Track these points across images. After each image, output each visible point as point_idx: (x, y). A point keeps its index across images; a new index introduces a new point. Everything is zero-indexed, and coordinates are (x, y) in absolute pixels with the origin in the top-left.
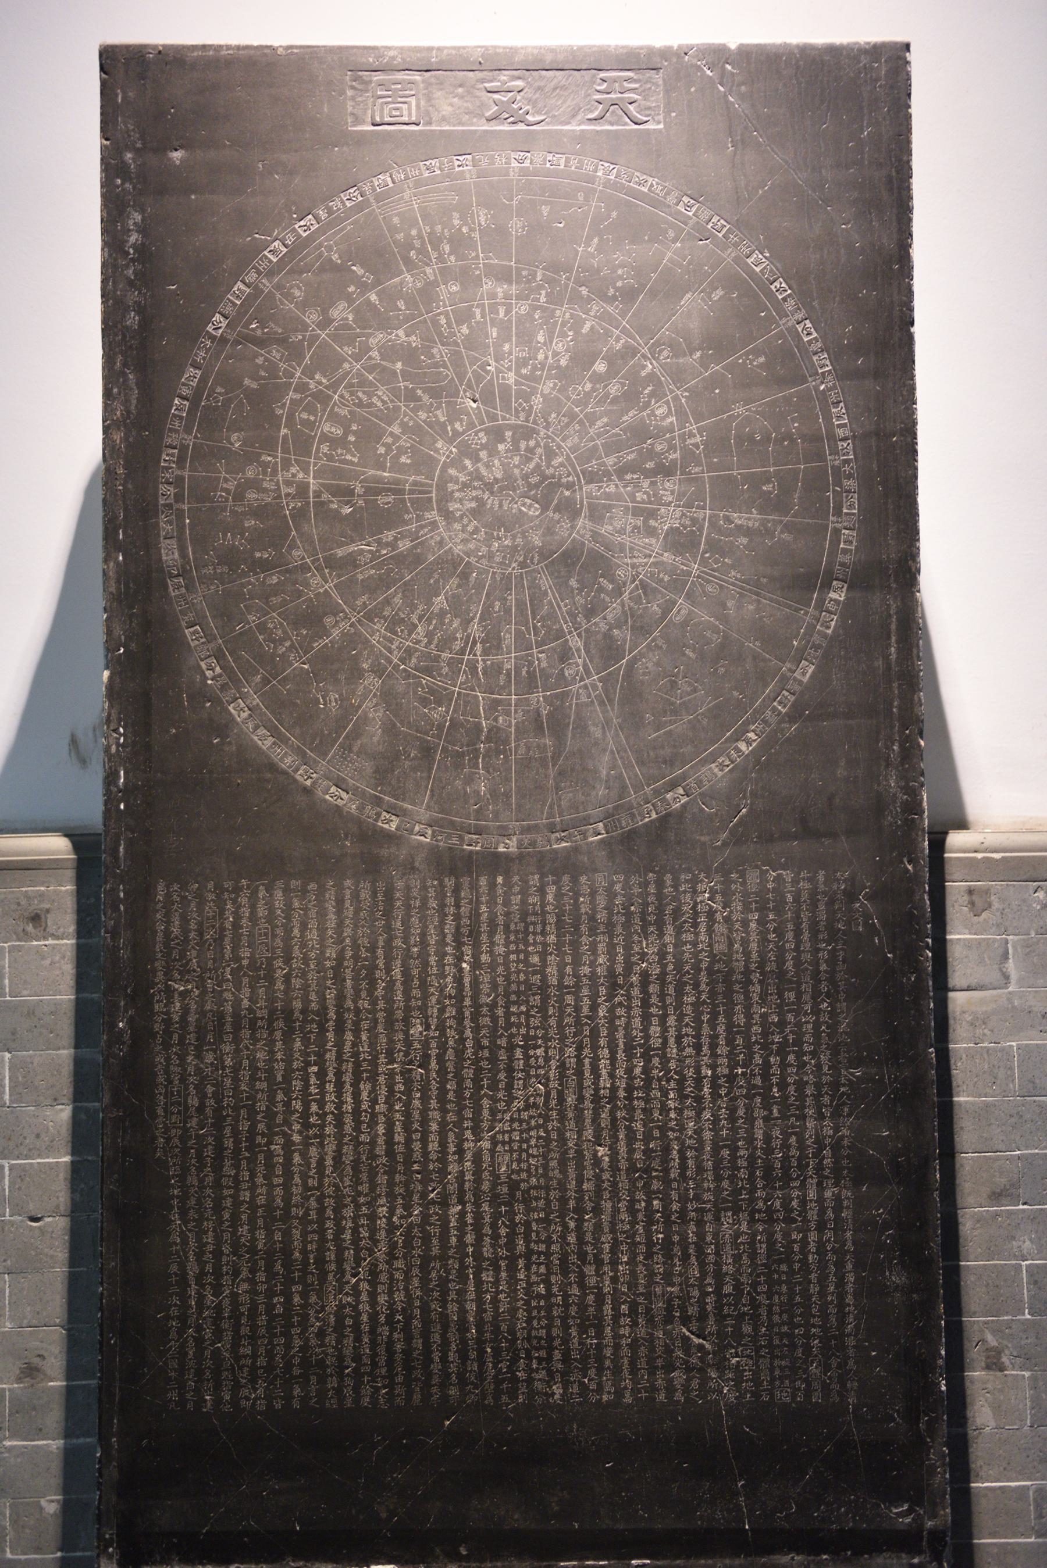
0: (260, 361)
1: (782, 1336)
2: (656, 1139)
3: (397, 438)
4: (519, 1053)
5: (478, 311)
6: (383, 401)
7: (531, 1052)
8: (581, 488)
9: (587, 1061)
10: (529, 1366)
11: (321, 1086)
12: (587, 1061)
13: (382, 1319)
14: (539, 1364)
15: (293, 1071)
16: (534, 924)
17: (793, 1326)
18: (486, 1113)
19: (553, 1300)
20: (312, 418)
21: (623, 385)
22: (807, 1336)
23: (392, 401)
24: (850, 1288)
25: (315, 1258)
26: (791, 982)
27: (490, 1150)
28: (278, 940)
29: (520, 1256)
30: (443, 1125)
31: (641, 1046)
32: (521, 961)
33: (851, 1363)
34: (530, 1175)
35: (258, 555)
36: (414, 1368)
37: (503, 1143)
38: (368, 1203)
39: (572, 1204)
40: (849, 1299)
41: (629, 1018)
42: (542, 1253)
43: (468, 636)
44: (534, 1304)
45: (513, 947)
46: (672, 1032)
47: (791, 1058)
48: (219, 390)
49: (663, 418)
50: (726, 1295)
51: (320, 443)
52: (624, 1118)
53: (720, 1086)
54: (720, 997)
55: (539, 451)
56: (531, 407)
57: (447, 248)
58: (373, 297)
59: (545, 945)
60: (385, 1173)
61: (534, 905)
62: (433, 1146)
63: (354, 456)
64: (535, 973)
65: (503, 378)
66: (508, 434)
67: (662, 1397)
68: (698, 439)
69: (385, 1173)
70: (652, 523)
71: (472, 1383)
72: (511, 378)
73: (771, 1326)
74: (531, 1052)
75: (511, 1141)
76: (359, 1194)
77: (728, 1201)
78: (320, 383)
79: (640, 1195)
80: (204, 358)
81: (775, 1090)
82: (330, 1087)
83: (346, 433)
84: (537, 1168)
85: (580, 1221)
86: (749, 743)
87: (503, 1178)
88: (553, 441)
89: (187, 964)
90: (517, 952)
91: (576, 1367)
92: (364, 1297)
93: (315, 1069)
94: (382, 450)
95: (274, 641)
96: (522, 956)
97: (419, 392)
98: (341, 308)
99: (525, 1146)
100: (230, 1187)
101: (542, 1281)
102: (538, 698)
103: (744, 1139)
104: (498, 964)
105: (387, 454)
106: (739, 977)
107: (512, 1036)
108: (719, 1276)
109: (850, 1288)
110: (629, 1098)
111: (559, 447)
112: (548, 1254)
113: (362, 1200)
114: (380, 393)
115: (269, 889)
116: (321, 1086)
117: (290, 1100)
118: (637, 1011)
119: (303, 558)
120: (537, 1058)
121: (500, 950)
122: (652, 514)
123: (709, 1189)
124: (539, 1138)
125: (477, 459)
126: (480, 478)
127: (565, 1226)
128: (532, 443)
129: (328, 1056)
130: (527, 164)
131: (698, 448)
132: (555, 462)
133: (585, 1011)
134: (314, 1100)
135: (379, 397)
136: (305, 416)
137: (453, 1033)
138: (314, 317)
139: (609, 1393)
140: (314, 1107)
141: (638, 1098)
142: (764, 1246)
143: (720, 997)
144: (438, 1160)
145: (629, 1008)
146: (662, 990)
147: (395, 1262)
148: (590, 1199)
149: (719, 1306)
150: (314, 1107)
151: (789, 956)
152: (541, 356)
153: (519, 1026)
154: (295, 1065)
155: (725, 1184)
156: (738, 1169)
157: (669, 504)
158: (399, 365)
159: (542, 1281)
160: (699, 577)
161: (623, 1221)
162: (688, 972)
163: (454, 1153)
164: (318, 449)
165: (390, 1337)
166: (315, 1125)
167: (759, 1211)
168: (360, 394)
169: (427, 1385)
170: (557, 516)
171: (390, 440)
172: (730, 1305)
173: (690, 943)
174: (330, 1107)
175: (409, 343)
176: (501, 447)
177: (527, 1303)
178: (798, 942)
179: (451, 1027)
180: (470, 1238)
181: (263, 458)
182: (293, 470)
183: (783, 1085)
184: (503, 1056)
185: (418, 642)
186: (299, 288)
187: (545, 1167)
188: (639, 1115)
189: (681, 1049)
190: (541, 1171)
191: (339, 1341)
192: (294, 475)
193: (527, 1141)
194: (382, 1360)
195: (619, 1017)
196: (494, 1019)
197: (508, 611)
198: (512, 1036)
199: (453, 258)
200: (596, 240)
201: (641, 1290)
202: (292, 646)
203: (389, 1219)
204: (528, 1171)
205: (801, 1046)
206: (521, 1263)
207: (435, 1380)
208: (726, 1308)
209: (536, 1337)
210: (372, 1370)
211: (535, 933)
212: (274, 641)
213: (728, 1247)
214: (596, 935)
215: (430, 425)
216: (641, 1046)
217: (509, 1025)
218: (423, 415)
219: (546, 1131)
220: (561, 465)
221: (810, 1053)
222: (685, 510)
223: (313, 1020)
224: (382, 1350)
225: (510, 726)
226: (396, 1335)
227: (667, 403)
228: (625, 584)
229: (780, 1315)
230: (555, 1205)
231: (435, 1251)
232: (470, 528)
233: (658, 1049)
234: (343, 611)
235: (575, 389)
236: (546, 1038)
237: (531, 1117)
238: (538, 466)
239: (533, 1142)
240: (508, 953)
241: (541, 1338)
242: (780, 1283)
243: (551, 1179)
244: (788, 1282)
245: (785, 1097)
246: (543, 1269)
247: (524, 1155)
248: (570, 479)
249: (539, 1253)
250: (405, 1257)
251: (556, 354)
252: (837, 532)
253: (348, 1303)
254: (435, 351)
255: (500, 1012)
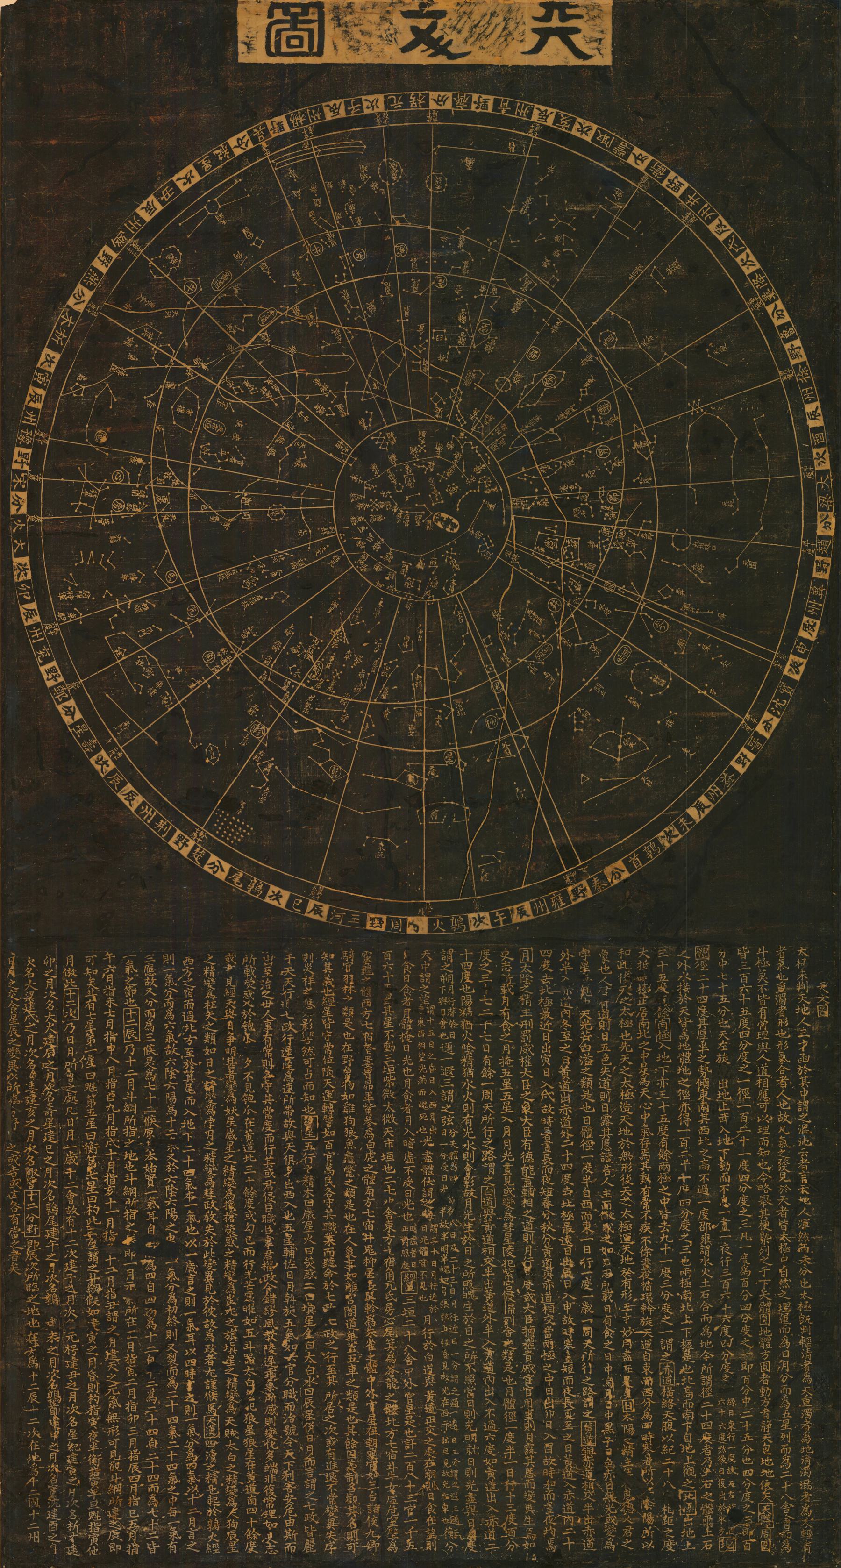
0: (129, 343)
1: (728, 1477)
2: (587, 1256)
3: (291, 437)
4: (428, 1157)
5: (388, 286)
6: (273, 392)
7: (444, 1156)
8: (507, 502)
9: (507, 1166)
10: (439, 1510)
11: (199, 1193)
12: (507, 1166)
13: (270, 1455)
14: (450, 1508)
15: (167, 1175)
16: (446, 1007)
17: (741, 1467)
18: (389, 1225)
19: (467, 1437)
20: (190, 412)
21: (559, 376)
22: (757, 1478)
23: (284, 392)
24: (807, 1426)
25: (194, 1386)
26: (745, 1076)
27: (394, 1269)
28: (149, 1023)
29: (429, 1388)
30: (340, 1238)
31: (570, 1149)
32: (432, 1051)
33: (805, 1508)
34: (440, 1297)
35: (125, 577)
36: (307, 1511)
37: (410, 1260)
38: (253, 1326)
39: (489, 1329)
40: (807, 1438)
41: (558, 1116)
42: (454, 1385)
43: (373, 676)
44: (445, 1441)
45: (421, 1033)
46: (606, 1134)
47: (744, 1164)
48: (81, 377)
49: (606, 418)
50: (665, 1433)
51: (199, 443)
52: (550, 1232)
53: (661, 1196)
54: (662, 1093)
55: (458, 455)
56: (449, 402)
57: (352, 208)
58: (264, 266)
59: (459, 1031)
60: (273, 1291)
61: (448, 984)
62: (329, 1262)
63: (239, 459)
64: (449, 1063)
65: (417, 366)
66: (422, 434)
67: (590, 1543)
68: (648, 443)
69: (273, 1291)
70: (592, 544)
71: (373, 1528)
72: (426, 365)
73: (716, 1466)
74: (444, 1156)
75: (419, 1257)
76: (243, 1315)
77: (669, 1328)
78: (200, 370)
79: (569, 1320)
80: (64, 340)
81: (725, 1200)
82: (209, 1193)
83: (230, 431)
84: (448, 1287)
85: (499, 1349)
86: (700, 808)
87: (410, 1300)
88: (476, 443)
89: (44, 1051)
90: (426, 1040)
91: (493, 1512)
92: (250, 1430)
93: (192, 1172)
94: (272, 452)
95: (142, 681)
96: (432, 1045)
97: (317, 381)
98: (225, 277)
99: (434, 1263)
100: (95, 1307)
101: (454, 1416)
102: (453, 754)
103: (688, 1256)
104: (404, 1054)
105: (278, 457)
106: (686, 1069)
107: (420, 1137)
108: (658, 1413)
109: (807, 1426)
110: (557, 1209)
111: (483, 450)
112: (461, 1386)
113: (247, 1321)
114: (269, 382)
115: (139, 964)
116: (199, 1193)
117: (164, 1207)
118: (566, 1109)
119: (179, 582)
120: (449, 1162)
121: (407, 1036)
122: (593, 534)
123: (647, 1313)
124: (451, 1254)
125: (384, 464)
126: (390, 487)
127: (481, 1355)
128: (450, 446)
129: (207, 1158)
130: (448, 105)
131: (647, 454)
132: (477, 470)
133: (507, 1108)
134: (192, 1208)
135: (269, 387)
136: (181, 410)
137: (352, 1132)
138: (193, 288)
139: (530, 1541)
140: (191, 1217)
141: (567, 1209)
142: (710, 1378)
143: (662, 1093)
144: (334, 1278)
145: (557, 1106)
146: (595, 1085)
147: (286, 1392)
148: (510, 1324)
149: (656, 1443)
150: (191, 1217)
151: (743, 1046)
152: (462, 341)
153: (428, 1124)
154: (169, 1168)
155: (666, 1307)
156: (681, 1291)
157: (612, 522)
158: (293, 349)
159: (454, 1416)
160: (645, 610)
161: (547, 1350)
162: (626, 1064)
163: (353, 1271)
164: (197, 449)
165: (279, 1476)
166: (192, 1237)
167: (705, 1339)
168: (247, 384)
169: (321, 1530)
170: (479, 535)
171: (281, 440)
172: (669, 1444)
173: (629, 1030)
174: (210, 1216)
175: (305, 322)
176: (413, 450)
177: (437, 1440)
178: (755, 1029)
179: (349, 1126)
180: (371, 1367)
181: (133, 460)
182: (168, 475)
183: (734, 1195)
184: (410, 1158)
185: (313, 683)
186: (176, 254)
187: (459, 1288)
188: (568, 1229)
189: (616, 1153)
190: (453, 1292)
191: (221, 1479)
192: (168, 482)
193: (438, 1257)
194: (270, 1500)
195: (546, 1116)
196: (400, 1115)
197: (419, 646)
198: (420, 1137)
199: (359, 220)
200: (529, 200)
201: (568, 1426)
202: (165, 687)
203: (278, 1344)
204: (438, 1292)
205: (755, 1150)
206: (430, 1396)
207: (331, 1524)
208: (665, 1447)
209: (446, 1478)
210: (259, 1512)
211: (448, 1018)
212: (142, 681)
213: (669, 1378)
214: (520, 1020)
215: (330, 421)
216: (570, 1149)
217: (417, 1124)
218: (320, 409)
219: (459, 1245)
220: (484, 472)
221: (766, 1159)
222: (630, 530)
223: (189, 1116)
224: (270, 1490)
225: (420, 785)
226: (286, 1474)
227: (611, 399)
228: (558, 616)
229: (726, 1456)
230: (469, 1331)
231: (331, 1380)
232: (376, 547)
233: (590, 1152)
234: (225, 645)
235: (503, 381)
236: (460, 1139)
237: (441, 1231)
238: (457, 472)
239: (444, 1259)
240: (415, 1041)
241: (453, 1479)
242: (726, 1419)
243: (465, 1301)
244: (737, 1419)
245: (735, 1209)
246: (456, 1404)
247: (434, 1274)
248: (495, 489)
249: (451, 1385)
250: (297, 1386)
251: (480, 338)
252: (809, 560)
253: (232, 1437)
254: (336, 332)
255: (407, 1109)
